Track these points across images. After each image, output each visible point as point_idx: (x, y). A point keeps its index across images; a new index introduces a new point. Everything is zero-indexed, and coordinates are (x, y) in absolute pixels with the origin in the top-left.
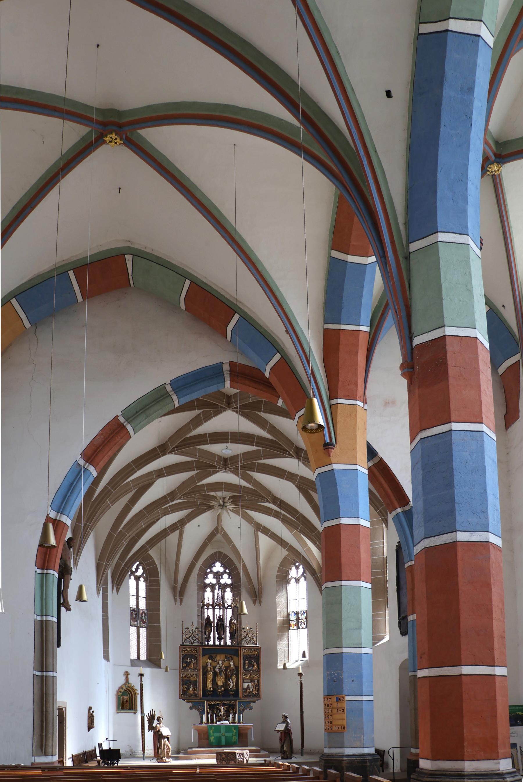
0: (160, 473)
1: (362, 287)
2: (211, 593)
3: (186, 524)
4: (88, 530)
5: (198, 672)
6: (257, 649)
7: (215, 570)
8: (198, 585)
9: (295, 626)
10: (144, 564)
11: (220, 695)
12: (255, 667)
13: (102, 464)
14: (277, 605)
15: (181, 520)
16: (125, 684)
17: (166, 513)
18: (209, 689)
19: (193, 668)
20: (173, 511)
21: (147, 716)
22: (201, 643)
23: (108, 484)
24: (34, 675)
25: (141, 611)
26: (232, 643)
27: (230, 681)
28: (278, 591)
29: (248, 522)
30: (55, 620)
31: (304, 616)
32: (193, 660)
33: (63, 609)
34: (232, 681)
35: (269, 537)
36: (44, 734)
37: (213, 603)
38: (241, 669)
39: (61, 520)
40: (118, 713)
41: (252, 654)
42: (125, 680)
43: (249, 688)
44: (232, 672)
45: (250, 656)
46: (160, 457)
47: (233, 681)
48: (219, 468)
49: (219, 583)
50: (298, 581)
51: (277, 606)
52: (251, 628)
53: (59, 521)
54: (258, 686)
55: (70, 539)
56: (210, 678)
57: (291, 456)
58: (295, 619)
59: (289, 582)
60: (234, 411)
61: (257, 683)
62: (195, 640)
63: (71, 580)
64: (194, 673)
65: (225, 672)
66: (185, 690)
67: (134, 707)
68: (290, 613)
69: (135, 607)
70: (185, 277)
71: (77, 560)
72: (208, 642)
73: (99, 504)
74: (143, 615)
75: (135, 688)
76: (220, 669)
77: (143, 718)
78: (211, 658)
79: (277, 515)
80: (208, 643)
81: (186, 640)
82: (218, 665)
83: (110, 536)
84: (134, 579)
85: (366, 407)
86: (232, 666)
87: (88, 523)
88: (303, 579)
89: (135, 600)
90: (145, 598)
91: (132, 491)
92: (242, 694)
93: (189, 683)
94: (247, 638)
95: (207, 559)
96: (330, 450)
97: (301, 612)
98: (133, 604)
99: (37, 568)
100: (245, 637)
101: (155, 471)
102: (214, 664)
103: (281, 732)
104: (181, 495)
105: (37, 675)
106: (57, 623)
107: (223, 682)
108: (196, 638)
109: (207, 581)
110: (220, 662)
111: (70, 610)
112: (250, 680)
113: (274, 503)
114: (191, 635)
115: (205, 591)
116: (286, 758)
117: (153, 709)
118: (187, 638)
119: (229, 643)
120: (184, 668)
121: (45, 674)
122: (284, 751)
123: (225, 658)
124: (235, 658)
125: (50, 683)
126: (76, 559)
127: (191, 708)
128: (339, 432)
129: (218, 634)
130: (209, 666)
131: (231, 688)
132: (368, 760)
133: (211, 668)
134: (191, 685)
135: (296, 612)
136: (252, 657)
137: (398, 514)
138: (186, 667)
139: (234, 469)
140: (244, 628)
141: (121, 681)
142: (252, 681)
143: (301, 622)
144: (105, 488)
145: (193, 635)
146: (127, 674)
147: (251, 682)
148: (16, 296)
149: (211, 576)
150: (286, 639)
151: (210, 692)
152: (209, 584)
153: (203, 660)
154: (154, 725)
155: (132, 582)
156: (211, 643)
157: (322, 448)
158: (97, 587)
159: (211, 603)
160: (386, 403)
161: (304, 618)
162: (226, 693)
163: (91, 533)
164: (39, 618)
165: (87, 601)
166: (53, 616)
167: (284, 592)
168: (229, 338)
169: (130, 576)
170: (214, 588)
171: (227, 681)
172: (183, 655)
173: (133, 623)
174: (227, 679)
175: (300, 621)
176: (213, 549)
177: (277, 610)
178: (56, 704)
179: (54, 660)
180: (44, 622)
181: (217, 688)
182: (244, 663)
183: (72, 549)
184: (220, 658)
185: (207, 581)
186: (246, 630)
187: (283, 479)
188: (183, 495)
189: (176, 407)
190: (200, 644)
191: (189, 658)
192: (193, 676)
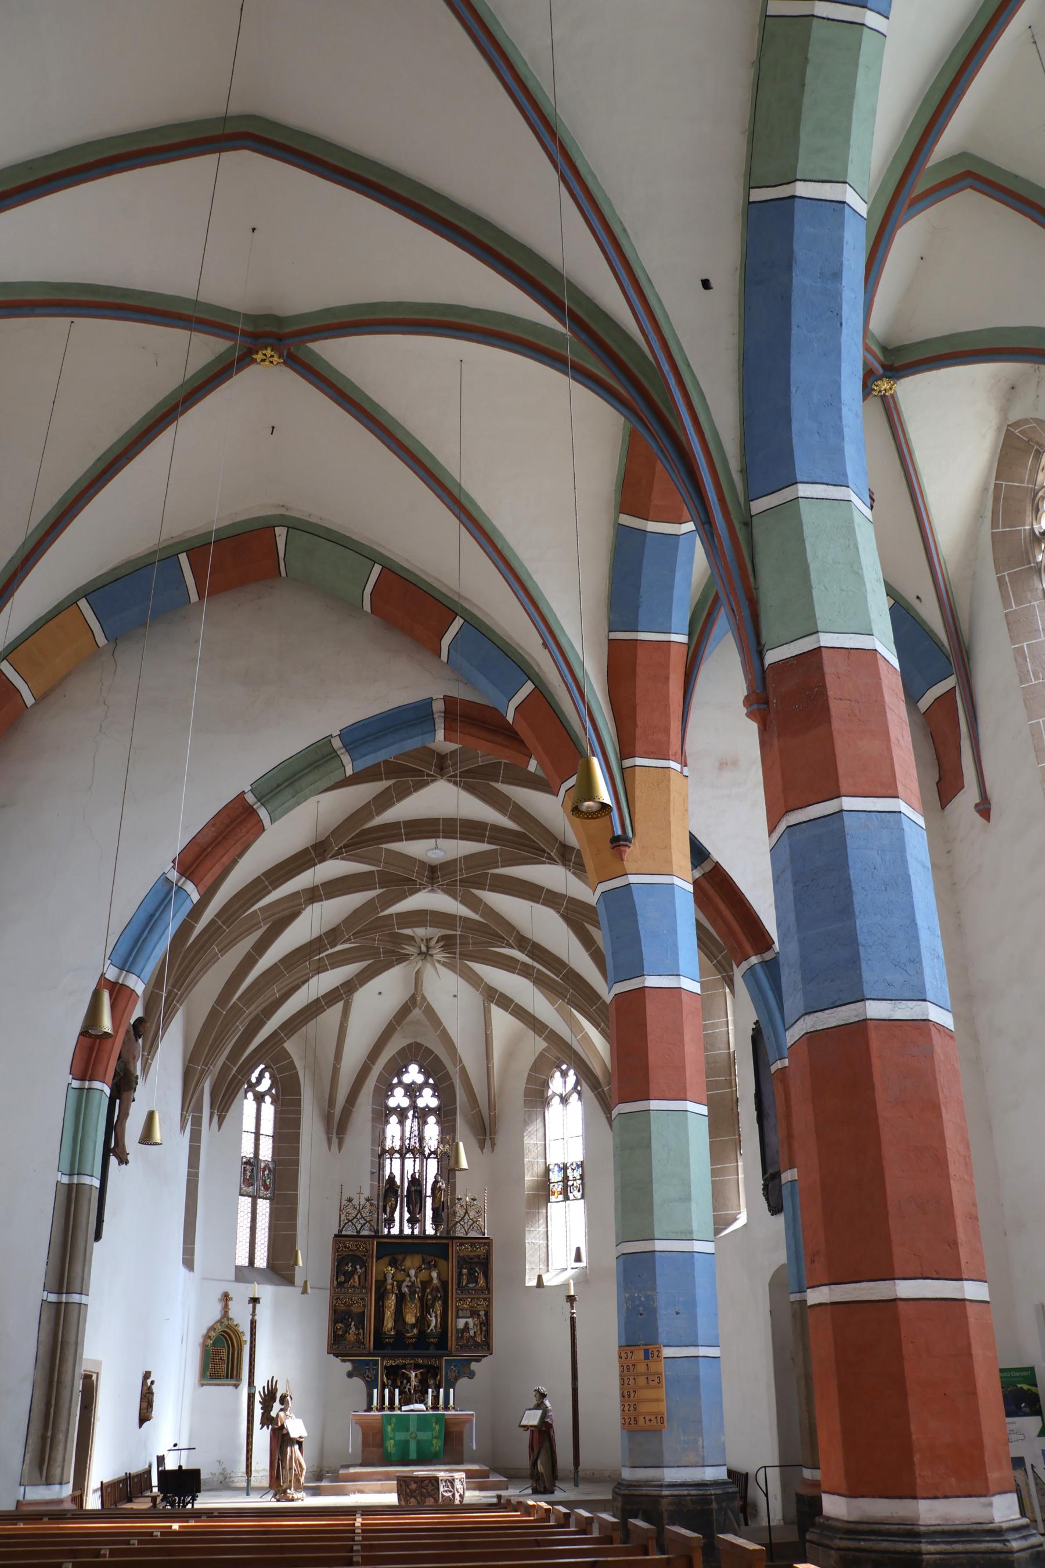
0: (314, 895)
1: (673, 571)
5: (367, 1294)
6: (485, 1244)
7: (407, 1079)
8: (374, 1111)
9: (561, 1194)
10: (273, 1069)
11: (409, 1344)
12: (482, 1282)
13: (209, 879)
14: (526, 1152)
16: (220, 1321)
17: (320, 969)
19: (357, 1284)
20: (334, 965)
21: (259, 1392)
25: (263, 1165)
26: (436, 1230)
27: (430, 1314)
28: (527, 1122)
29: (471, 984)
30: (97, 1183)
31: (577, 1174)
32: (358, 1267)
33: (113, 1160)
34: (433, 1315)
35: (510, 1013)
36: (49, 1434)
37: (401, 1147)
38: (452, 1287)
39: (126, 983)
40: (202, 1385)
41: (476, 1254)
42: (221, 1311)
43: (468, 1328)
44: (434, 1293)
45: (471, 1259)
46: (315, 865)
47: (436, 1313)
48: (420, 884)
49: (414, 1106)
50: (567, 1101)
51: (525, 1152)
52: (474, 1200)
53: (122, 985)
54: (486, 1325)
55: (139, 1021)
56: (391, 1307)
57: (552, 861)
58: (560, 1179)
59: (549, 1103)
60: (450, 781)
61: (484, 1318)
62: (364, 1224)
63: (134, 1100)
64: (361, 1296)
65: (420, 1294)
66: (340, 1333)
68: (551, 1167)
69: (252, 1156)
71: (149, 1061)
72: (389, 1229)
73: (198, 952)
74: (267, 1172)
78: (393, 1263)
79: (525, 971)
82: (408, 1279)
86: (435, 1281)
88: (575, 1096)
89: (253, 1141)
90: (272, 1137)
93: (349, 1318)
94: (466, 1221)
95: (393, 1057)
96: (622, 848)
97: (572, 1164)
98: (247, 1150)
99: (73, 1078)
100: (463, 1219)
101: (305, 891)
102: (400, 1276)
106: (98, 1190)
108: (365, 1220)
109: (392, 1103)
110: (412, 1272)
111: (127, 1163)
112: (471, 1311)
113: (521, 949)
115: (387, 1122)
117: (273, 1377)
118: (349, 1221)
119: (430, 1230)
120: (340, 1284)
122: (538, 1473)
123: (421, 1263)
124: (442, 1263)
126: (147, 1059)
127: (350, 1375)
128: (637, 817)
129: (409, 1211)
130: (390, 1281)
131: (432, 1330)
132: (713, 1497)
133: (393, 1284)
134: (353, 1323)
136: (476, 1260)
138: (344, 1282)
139: (447, 885)
140: (461, 1199)
141: (214, 1314)
142: (474, 1314)
143: (573, 1185)
144: (212, 922)
145: (361, 1214)
146: (226, 1298)
147: (471, 1316)
148: (87, 595)
149: (399, 1092)
150: (542, 1221)
151: (389, 1338)
152: (395, 1109)
154: (273, 1414)
155: (249, 1104)
156: (395, 1231)
158: (182, 1114)
159: (397, 1148)
160: (721, 764)
161: (578, 1177)
164: (65, 1180)
167: (539, 1123)
169: (246, 1092)
170: (404, 1116)
172: (340, 1257)
174: (425, 1308)
175: (570, 1183)
176: (404, 1037)
177: (526, 1160)
179: (86, 1269)
182: (460, 1275)
183: (140, 1041)
185: (392, 1103)
186: (464, 1203)
188: (353, 935)
190: (373, 1234)
191: (350, 1264)
192: (357, 1302)
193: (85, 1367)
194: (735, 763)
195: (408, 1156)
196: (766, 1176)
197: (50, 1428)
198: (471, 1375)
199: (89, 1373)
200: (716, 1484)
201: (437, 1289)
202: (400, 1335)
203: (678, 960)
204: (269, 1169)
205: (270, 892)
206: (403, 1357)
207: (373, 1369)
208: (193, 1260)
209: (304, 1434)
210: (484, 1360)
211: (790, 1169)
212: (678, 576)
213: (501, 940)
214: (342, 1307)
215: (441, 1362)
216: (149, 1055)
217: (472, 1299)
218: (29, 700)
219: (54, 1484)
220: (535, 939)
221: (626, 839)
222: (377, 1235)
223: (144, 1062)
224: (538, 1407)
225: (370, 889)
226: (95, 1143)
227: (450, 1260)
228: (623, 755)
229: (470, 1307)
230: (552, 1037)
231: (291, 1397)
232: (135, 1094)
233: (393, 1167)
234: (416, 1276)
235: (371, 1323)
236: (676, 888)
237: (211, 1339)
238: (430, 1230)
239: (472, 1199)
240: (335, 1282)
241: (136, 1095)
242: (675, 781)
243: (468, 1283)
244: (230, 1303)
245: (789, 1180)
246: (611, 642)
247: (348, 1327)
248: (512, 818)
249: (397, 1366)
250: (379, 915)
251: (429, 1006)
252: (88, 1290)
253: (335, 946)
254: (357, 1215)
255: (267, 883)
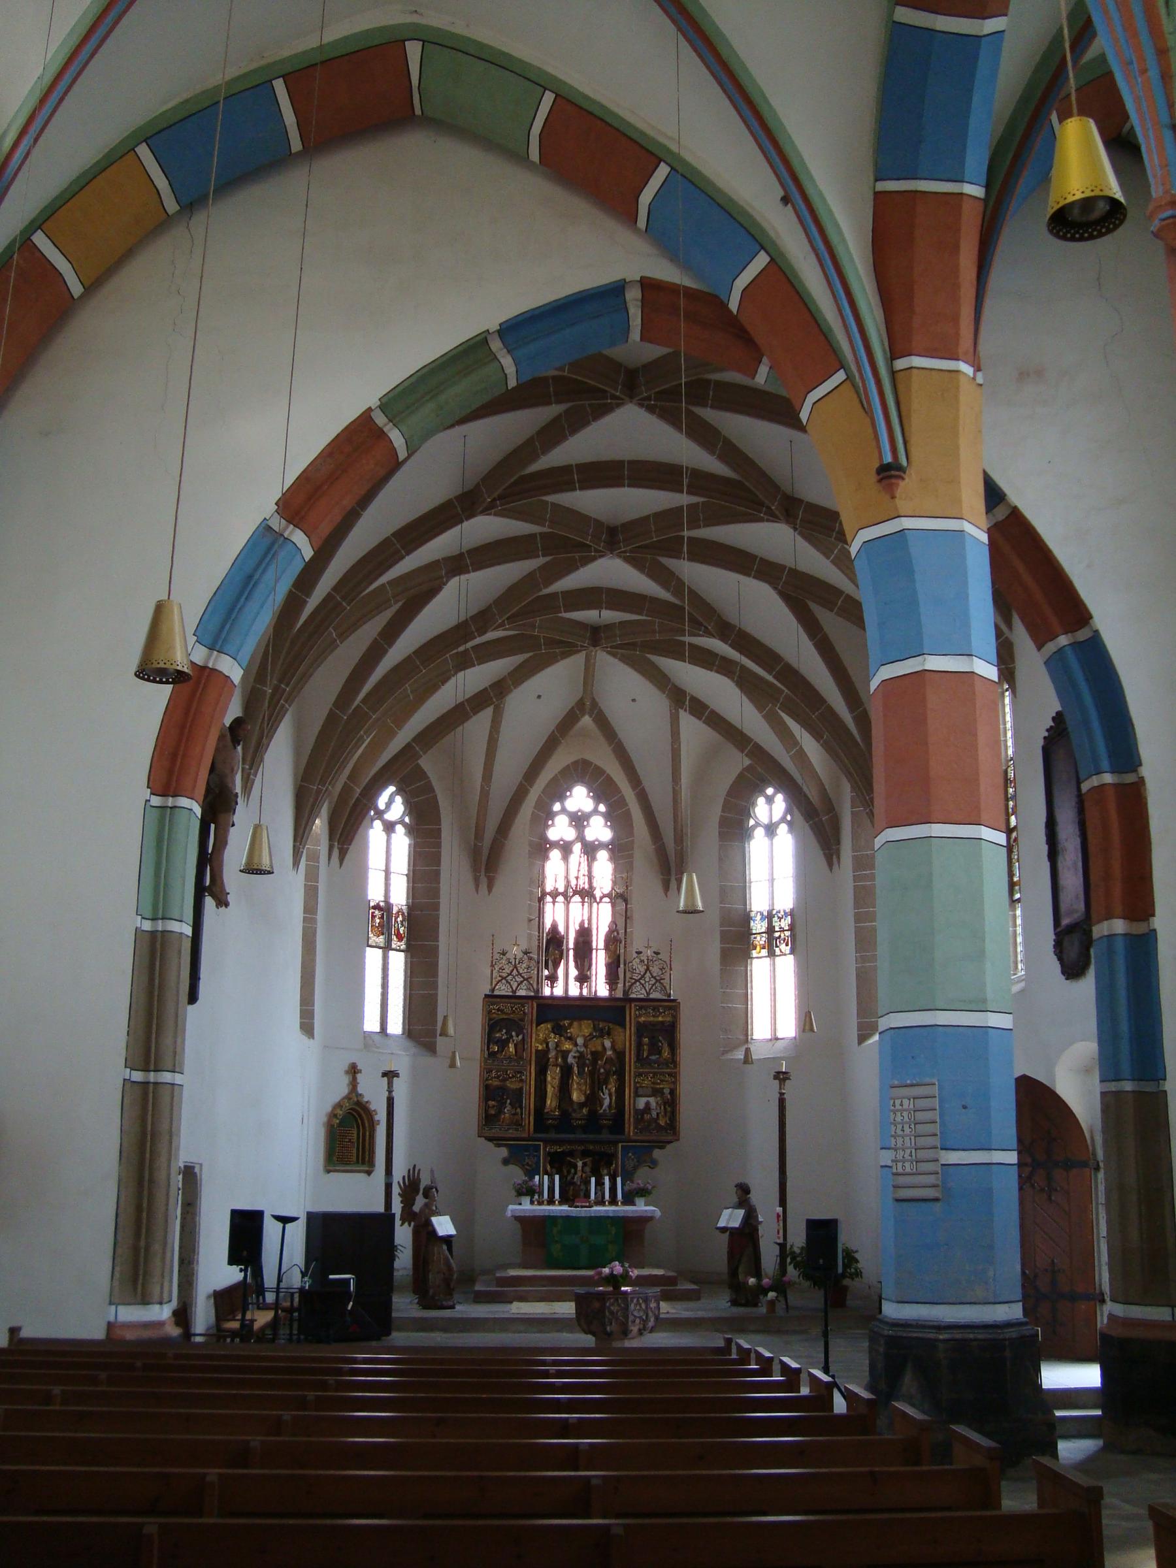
0: (458, 564)
1: (970, 91)
2: (562, 864)
3: (510, 691)
4: (282, 701)
6: (670, 1008)
12: (666, 1054)
13: (325, 529)
15: (499, 681)
16: (348, 1097)
17: (464, 662)
18: (551, 1111)
20: (482, 660)
21: (399, 1182)
22: (534, 992)
23: (336, 588)
24: (125, 1080)
26: (611, 990)
30: (188, 931)
31: (785, 923)
32: (514, 1033)
33: (209, 902)
34: (606, 1092)
35: (704, 722)
36: (142, 1243)
37: (566, 891)
38: (630, 1058)
39: (216, 668)
40: (329, 1172)
42: (348, 1085)
43: (649, 1109)
44: (608, 1066)
46: (461, 522)
48: (596, 551)
49: (581, 838)
52: (657, 953)
53: (214, 670)
54: (671, 1104)
55: (237, 722)
57: (773, 517)
58: (763, 930)
59: (750, 835)
60: (641, 405)
61: (669, 1097)
62: (522, 982)
63: (233, 825)
66: (492, 1112)
67: (367, 1159)
68: (753, 914)
70: (541, 86)
71: (252, 777)
72: (552, 987)
74: (400, 919)
75: (372, 1107)
76: (581, 1057)
77: (388, 1187)
78: (559, 1030)
79: (724, 667)
80: (552, 992)
81: (500, 981)
83: (331, 719)
84: (381, 827)
85: (980, 379)
87: (283, 686)
91: (391, 606)
92: (632, 1128)
94: (647, 980)
96: (893, 481)
97: (779, 912)
98: (375, 894)
99: (152, 793)
100: (643, 976)
101: (446, 559)
102: (567, 1046)
103: (732, 1232)
104: (504, 618)
105: (133, 1079)
106: (190, 939)
107: (585, 1094)
108: (523, 977)
109: (553, 834)
110: (580, 1041)
111: (227, 905)
113: (724, 639)
114: (511, 969)
115: (546, 858)
116: (743, 1302)
117: (415, 1166)
119: (603, 990)
120: (492, 1055)
121: (152, 1077)
125: (166, 1098)
126: (249, 775)
127: (506, 1162)
128: (914, 440)
129: (577, 967)
131: (604, 1111)
132: (1007, 1343)
134: (509, 1101)
135: (765, 914)
137: (1061, 650)
139: (631, 551)
140: (641, 953)
141: (340, 1089)
142: (656, 1092)
143: (780, 936)
144: (328, 598)
146: (353, 1070)
148: (148, 138)
153: (541, 1036)
154: (417, 1208)
156: (559, 991)
157: (873, 478)
158: (294, 846)
159: (561, 890)
160: (1021, 374)
161: (787, 928)
162: (593, 1121)
163: (287, 710)
164: (147, 926)
165: (270, 873)
166: (181, 921)
168: (642, 222)
169: (372, 820)
171: (596, 1089)
173: (375, 938)
174: (596, 1084)
175: (777, 935)
178: (177, 1159)
179: (179, 1040)
180: (159, 935)
181: (570, 1110)
182: (639, 1045)
183: (239, 748)
184: (581, 1031)
187: (748, 575)
188: (507, 619)
189: (509, 388)
190: (532, 994)
191: (504, 1031)
193: (184, 1157)
194: (1040, 373)
195: (574, 899)
196: (1058, 930)
197: (143, 1236)
198: (654, 1164)
199: (190, 1164)
200: (1009, 1325)
201: (609, 1060)
202: (565, 1116)
203: (969, 636)
204: (403, 914)
205: (402, 558)
206: (570, 1142)
207: (534, 1156)
208: (312, 1024)
209: (452, 1231)
210: (669, 1147)
211: (1107, 920)
212: (976, 99)
213: (698, 627)
214: (496, 1083)
215: (616, 1148)
216: (251, 769)
217: (655, 1074)
218: (76, 289)
219: (153, 1303)
220: (743, 627)
221: (900, 468)
222: (538, 998)
223: (245, 776)
224: (740, 1205)
225: (531, 558)
226: (183, 878)
227: (628, 1027)
228: (894, 354)
229: (653, 1083)
230: (758, 753)
231: (436, 1189)
232: (235, 817)
233: (553, 914)
234: (585, 1045)
235: (530, 1102)
236: (967, 537)
237: (338, 1119)
238: (603, 990)
239: (655, 953)
240: (486, 1052)
241: (237, 818)
242: (967, 396)
243: (650, 1054)
244: (359, 1076)
245: (1106, 934)
246: (878, 195)
247: (502, 1105)
248: (722, 458)
249: (563, 1152)
250: (541, 593)
251: (601, 713)
252: (182, 1064)
253: (485, 633)
254: (512, 971)
255: (398, 546)
